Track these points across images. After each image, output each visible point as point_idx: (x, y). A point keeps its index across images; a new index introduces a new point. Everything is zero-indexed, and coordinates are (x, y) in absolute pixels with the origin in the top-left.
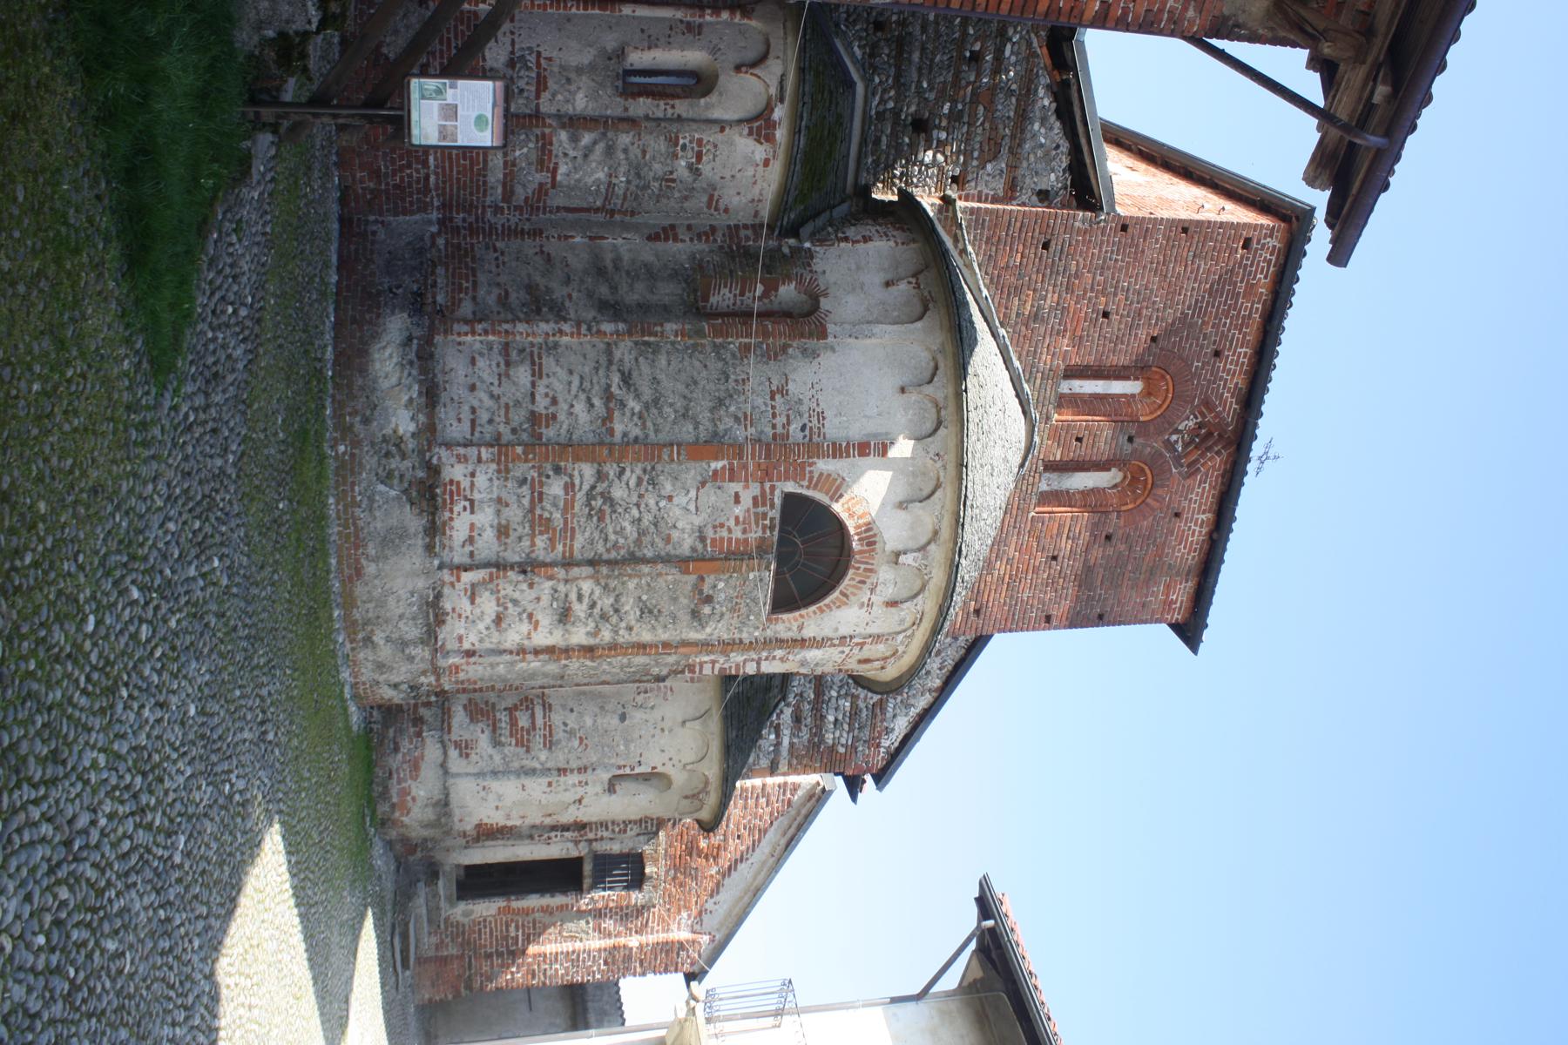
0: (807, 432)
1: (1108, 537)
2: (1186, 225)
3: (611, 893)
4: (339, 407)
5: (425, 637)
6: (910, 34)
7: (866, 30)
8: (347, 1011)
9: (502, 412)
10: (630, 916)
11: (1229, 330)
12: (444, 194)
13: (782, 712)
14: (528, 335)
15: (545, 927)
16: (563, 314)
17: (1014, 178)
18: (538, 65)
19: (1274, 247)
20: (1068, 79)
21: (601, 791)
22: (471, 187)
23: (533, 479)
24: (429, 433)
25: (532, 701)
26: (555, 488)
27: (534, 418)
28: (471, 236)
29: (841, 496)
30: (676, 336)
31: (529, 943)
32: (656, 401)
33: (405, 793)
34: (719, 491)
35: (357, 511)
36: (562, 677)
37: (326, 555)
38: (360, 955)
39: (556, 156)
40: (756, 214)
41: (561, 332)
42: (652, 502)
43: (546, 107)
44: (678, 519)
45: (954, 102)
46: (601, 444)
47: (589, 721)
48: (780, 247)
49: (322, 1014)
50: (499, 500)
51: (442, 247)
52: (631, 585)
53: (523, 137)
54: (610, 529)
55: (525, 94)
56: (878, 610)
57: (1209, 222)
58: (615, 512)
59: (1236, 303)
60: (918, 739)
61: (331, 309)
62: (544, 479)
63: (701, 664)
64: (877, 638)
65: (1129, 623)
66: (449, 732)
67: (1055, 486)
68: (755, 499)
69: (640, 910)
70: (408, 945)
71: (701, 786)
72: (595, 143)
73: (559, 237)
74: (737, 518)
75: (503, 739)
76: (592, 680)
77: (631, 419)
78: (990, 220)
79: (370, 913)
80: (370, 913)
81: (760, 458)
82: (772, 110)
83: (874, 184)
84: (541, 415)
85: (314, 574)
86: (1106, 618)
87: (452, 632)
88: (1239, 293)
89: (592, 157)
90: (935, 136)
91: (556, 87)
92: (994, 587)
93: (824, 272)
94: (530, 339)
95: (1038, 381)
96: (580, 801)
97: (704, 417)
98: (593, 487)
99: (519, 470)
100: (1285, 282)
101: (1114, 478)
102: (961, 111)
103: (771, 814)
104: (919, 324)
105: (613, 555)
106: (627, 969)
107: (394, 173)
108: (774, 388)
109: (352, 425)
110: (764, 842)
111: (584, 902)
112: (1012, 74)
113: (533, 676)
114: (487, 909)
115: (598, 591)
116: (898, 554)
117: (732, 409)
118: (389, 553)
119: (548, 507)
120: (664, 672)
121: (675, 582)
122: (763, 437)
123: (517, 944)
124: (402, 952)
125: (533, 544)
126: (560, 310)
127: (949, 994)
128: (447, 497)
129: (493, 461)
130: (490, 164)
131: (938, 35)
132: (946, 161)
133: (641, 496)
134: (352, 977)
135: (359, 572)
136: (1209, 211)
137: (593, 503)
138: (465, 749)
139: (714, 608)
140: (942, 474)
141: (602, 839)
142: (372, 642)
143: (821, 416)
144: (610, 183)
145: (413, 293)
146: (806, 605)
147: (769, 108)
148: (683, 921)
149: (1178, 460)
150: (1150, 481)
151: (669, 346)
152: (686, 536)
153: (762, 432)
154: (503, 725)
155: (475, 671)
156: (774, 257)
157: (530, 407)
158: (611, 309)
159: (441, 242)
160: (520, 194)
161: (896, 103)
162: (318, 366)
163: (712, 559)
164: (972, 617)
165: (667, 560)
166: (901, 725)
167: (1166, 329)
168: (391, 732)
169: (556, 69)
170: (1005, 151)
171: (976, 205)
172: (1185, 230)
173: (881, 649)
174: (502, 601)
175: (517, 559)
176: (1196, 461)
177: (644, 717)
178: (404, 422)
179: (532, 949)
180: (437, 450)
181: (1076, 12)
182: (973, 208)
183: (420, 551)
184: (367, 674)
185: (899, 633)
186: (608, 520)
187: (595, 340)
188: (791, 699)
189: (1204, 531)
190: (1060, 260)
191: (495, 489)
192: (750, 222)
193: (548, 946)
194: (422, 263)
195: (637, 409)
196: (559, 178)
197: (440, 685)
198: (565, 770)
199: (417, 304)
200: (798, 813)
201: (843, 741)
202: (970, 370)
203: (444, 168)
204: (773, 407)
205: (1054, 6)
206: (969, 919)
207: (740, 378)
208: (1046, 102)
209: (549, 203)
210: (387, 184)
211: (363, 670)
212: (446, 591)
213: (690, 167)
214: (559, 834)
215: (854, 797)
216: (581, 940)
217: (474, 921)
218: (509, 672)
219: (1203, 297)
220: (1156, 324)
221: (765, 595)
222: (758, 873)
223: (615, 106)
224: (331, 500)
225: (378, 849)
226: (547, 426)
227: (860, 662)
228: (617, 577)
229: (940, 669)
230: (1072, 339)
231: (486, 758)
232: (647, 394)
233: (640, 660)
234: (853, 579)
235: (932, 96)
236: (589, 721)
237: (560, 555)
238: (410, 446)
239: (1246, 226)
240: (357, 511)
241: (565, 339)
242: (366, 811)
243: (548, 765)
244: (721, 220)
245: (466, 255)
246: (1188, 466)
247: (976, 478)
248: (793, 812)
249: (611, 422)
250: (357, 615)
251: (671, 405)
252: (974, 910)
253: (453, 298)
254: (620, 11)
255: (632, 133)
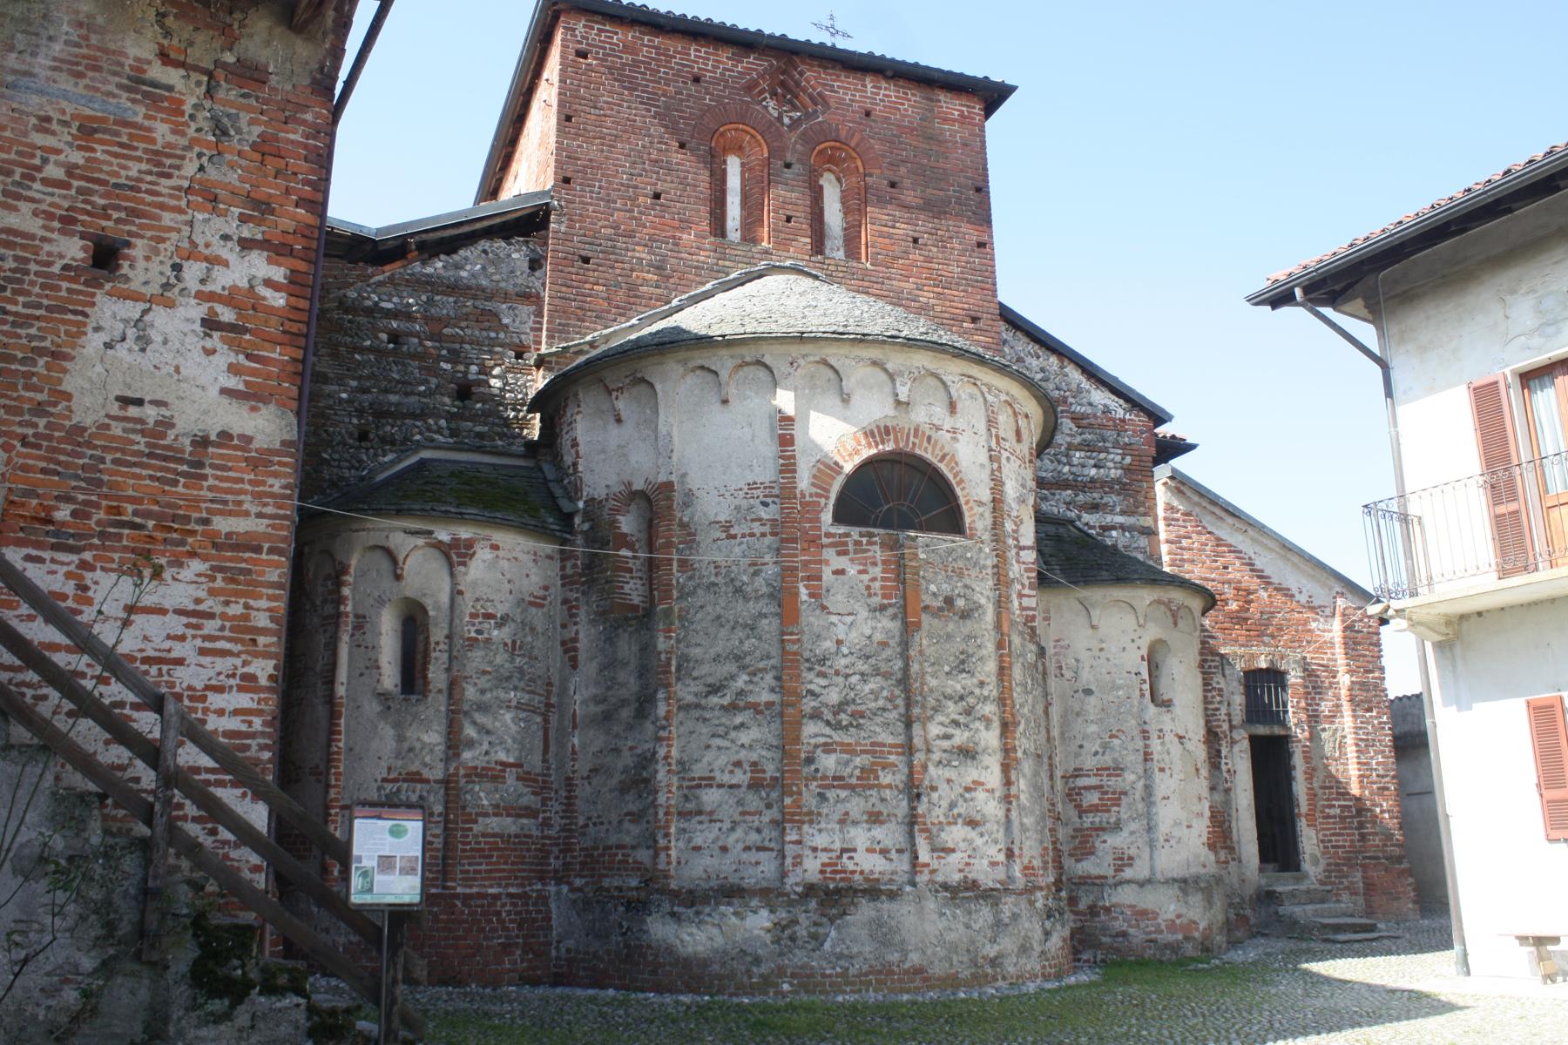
0: (769, 500)
1: (893, 185)
2: (563, 117)
3: (1290, 704)
4: (742, 989)
5: (990, 901)
6: (371, 404)
7: (367, 449)
8: (1404, 991)
9: (749, 818)
10: (1315, 685)
11: (672, 69)
12: (528, 878)
13: (1087, 524)
14: (670, 792)
15: (1330, 776)
16: (649, 755)
17: (517, 295)
18: (395, 780)
19: (584, 26)
20: (415, 243)
21: (1169, 716)
22: (522, 850)
23: (819, 786)
24: (770, 895)
25: (1070, 789)
26: (828, 763)
27: (755, 785)
28: (573, 851)
29: (836, 463)
30: (670, 638)
31: (1348, 794)
32: (738, 658)
33: (1172, 927)
34: (832, 592)
35: (852, 971)
36: (1039, 756)
37: (896, 1005)
38: (1347, 977)
39: (488, 762)
40: (549, 557)
41: (666, 757)
42: (843, 661)
43: (438, 773)
44: (862, 634)
45: (440, 358)
46: (781, 715)
47: (1093, 728)
48: (582, 532)
49: (1398, 1019)
50: (842, 822)
51: (583, 881)
52: (933, 683)
53: (468, 797)
54: (872, 705)
55: (425, 794)
56: (960, 422)
57: (560, 94)
58: (854, 700)
59: (643, 62)
60: (1115, 379)
61: (641, 996)
62: (819, 775)
63: (1023, 609)
64: (991, 422)
65: (985, 160)
66: (1105, 877)
67: (839, 242)
68: (839, 553)
69: (1309, 673)
70: (1348, 925)
71: (1163, 608)
72: (474, 723)
73: (574, 760)
74: (860, 572)
75: (1112, 820)
76: (1043, 724)
77: (757, 684)
78: (560, 318)
79: (1305, 966)
80: (1305, 966)
81: (796, 549)
82: (440, 542)
83: (524, 438)
84: (751, 778)
85: (911, 1017)
86: (980, 184)
87: (986, 873)
88: (633, 60)
89: (490, 726)
90: (475, 377)
91: (417, 763)
92: (948, 303)
93: (607, 486)
94: (674, 789)
95: (727, 263)
96: (1181, 737)
97: (753, 607)
98: (828, 723)
99: (809, 800)
100: (621, 12)
101: (830, 181)
102: (449, 351)
103: (1199, 533)
104: (658, 387)
105: (900, 702)
106: (1376, 686)
107: (505, 929)
108: (724, 535)
109: (761, 976)
110: (1230, 540)
111: (1301, 734)
112: (411, 301)
113: (1036, 787)
114: (1311, 838)
115: (940, 718)
116: (898, 403)
117: (745, 578)
118: (897, 939)
119: (849, 770)
120: (1033, 648)
121: (930, 636)
122: (775, 546)
123: (1350, 806)
124: (1355, 932)
125: (889, 786)
126: (646, 758)
127: (1382, 334)
128: (838, 876)
129: (799, 828)
130: (497, 830)
131: (372, 376)
132: (500, 365)
133: (837, 673)
134: (1369, 986)
135: (918, 971)
136: (550, 96)
137: (844, 723)
138: (1123, 861)
139: (959, 595)
140: (812, 359)
141: (1229, 715)
142: (996, 958)
143: (752, 486)
144: (516, 708)
145: (627, 911)
146: (955, 498)
147: (438, 546)
148: (1321, 627)
149: (808, 116)
150: (832, 144)
151: (681, 645)
152: (879, 625)
153: (769, 547)
154: (1097, 819)
155: (1031, 849)
156: (593, 538)
157: (744, 789)
158: (644, 705)
159: (578, 882)
160: (529, 800)
161: (441, 417)
162: (694, 1009)
163: (904, 598)
164: (980, 324)
165: (905, 645)
166: (1100, 397)
167: (672, 133)
168: (1104, 939)
169: (400, 763)
170: (489, 305)
171: (544, 333)
172: (568, 118)
173: (1004, 419)
174: (951, 820)
175: (905, 803)
176: (811, 96)
177: (1087, 669)
178: (759, 922)
179: (1355, 790)
180: (788, 887)
181: (307, 233)
182: (548, 336)
183: (894, 906)
184: (1032, 964)
185: (985, 399)
186: (863, 708)
187: (675, 722)
188: (1073, 515)
189: (884, 85)
190: (600, 245)
191: (829, 826)
192: (558, 564)
193: (1352, 772)
194: (598, 902)
195: (746, 678)
196: (511, 760)
197: (1048, 886)
198: (1146, 754)
199: (638, 907)
200: (1198, 504)
201: (1118, 458)
202: (703, 332)
203: (500, 878)
204: (743, 536)
205: (301, 255)
206: (1296, 316)
207: (713, 571)
208: (439, 265)
209: (538, 770)
210: (517, 936)
211: (1028, 968)
212: (940, 878)
213: (499, 625)
214: (1223, 761)
215: (1191, 447)
216: (1344, 737)
217: (1323, 853)
218: (1032, 812)
219: (637, 96)
220: (666, 144)
221: (944, 542)
222: (1266, 547)
223: (437, 704)
224: (840, 999)
225: (1237, 956)
226: (764, 771)
227: (1019, 440)
228: (925, 698)
229: (1038, 357)
230: (682, 230)
231: (1133, 838)
232: (731, 667)
233: (1017, 673)
234: (926, 450)
235: (434, 381)
236: (1093, 728)
237: (901, 758)
238: (784, 915)
239: (563, 56)
240: (852, 971)
241: (674, 752)
242: (1191, 968)
243: (1141, 772)
244: (557, 592)
245: (592, 856)
246: (816, 104)
247: (815, 323)
248: (1197, 510)
249: (759, 704)
250: (966, 973)
251: (741, 642)
252: (1285, 311)
253: (633, 869)
254: (341, 697)
255: (465, 685)
